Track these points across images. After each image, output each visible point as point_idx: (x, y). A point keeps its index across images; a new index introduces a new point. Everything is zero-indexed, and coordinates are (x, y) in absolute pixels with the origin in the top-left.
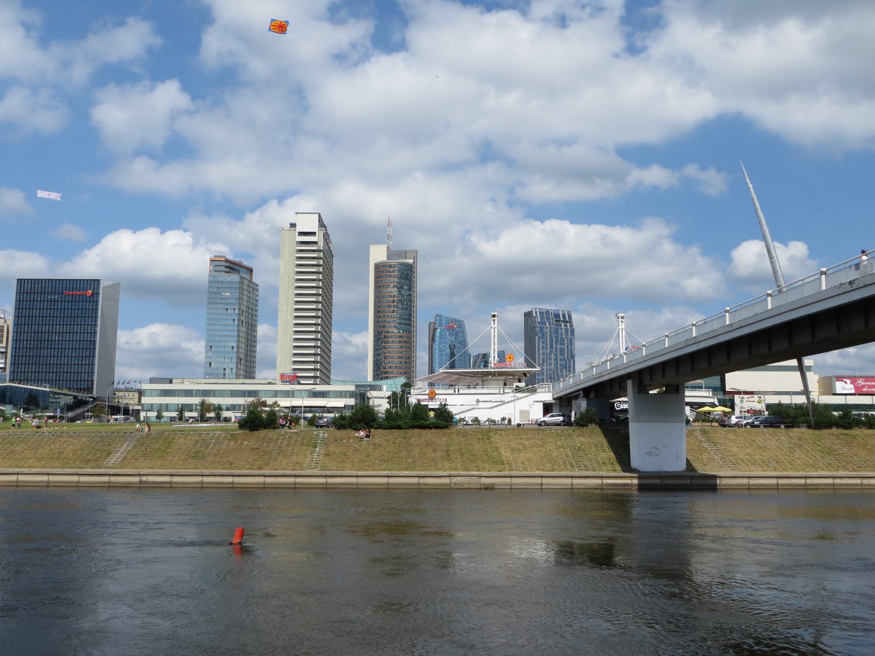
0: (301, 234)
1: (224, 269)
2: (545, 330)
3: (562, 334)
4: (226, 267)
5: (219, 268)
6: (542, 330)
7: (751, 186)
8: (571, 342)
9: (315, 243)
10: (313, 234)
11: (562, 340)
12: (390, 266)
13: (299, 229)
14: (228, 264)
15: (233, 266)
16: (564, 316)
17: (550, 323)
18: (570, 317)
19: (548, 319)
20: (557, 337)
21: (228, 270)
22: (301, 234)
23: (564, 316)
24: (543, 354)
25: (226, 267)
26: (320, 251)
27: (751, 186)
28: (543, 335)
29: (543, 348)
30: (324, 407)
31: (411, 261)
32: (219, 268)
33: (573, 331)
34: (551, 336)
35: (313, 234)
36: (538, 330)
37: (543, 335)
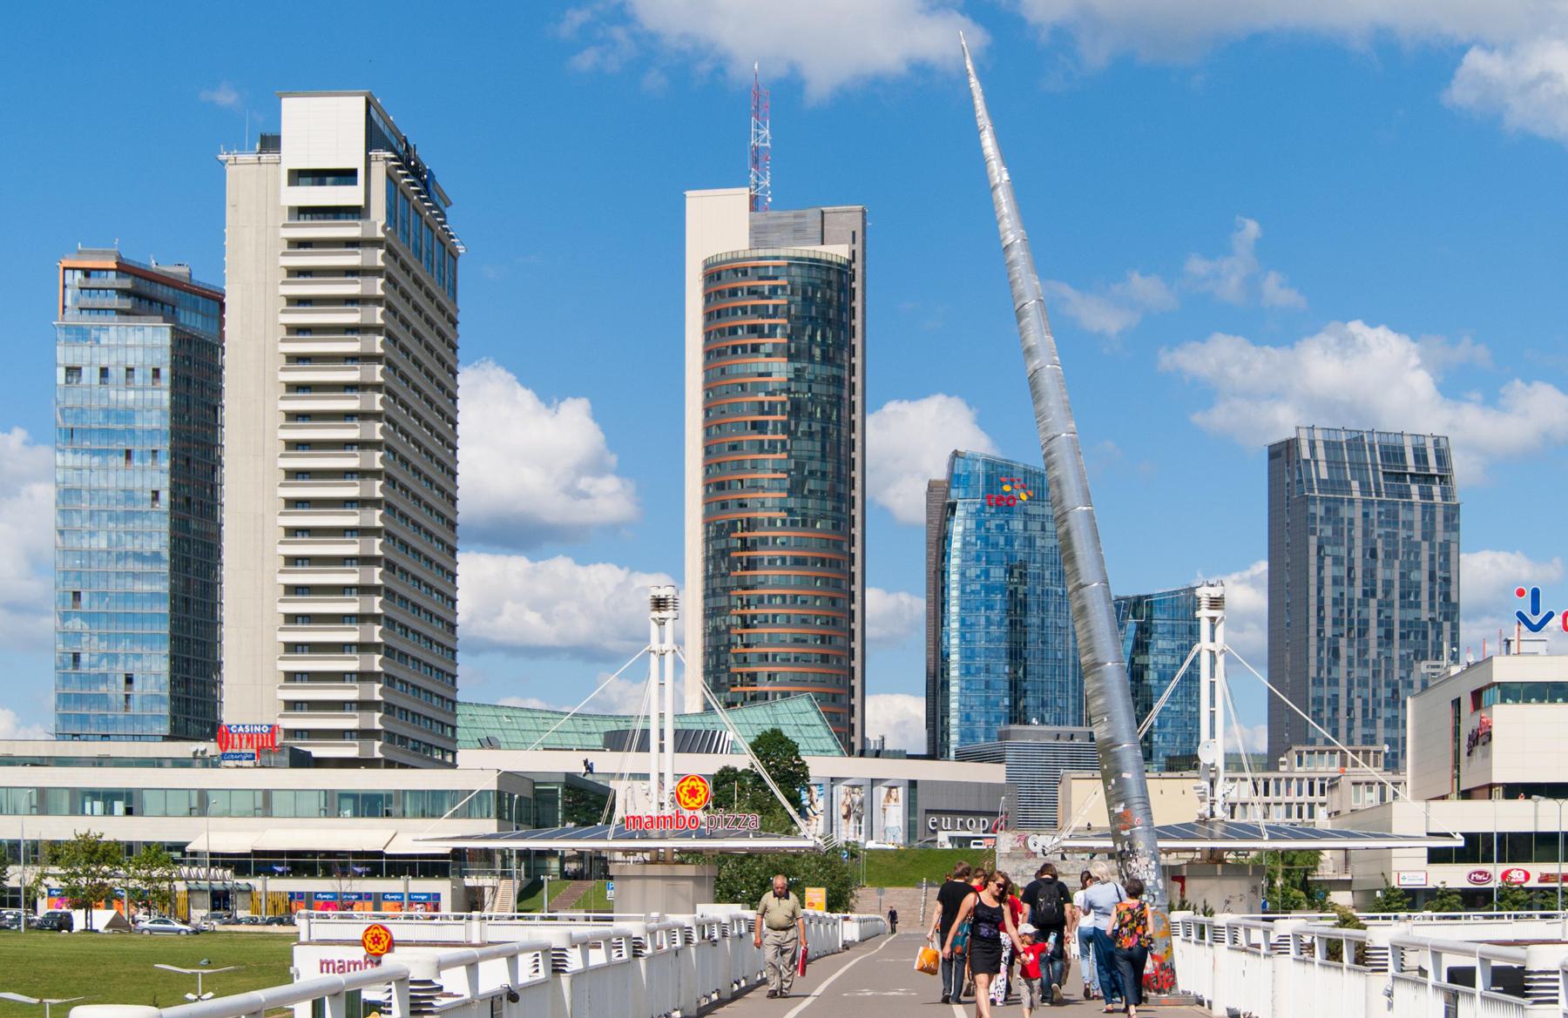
0: (299, 176)
1: (115, 301)
2: (1345, 512)
3: (1409, 525)
4: (123, 293)
5: (99, 301)
6: (1332, 513)
7: (999, 174)
8: (1446, 556)
10: (345, 176)
11: (1413, 548)
12: (760, 272)
13: (295, 155)
14: (127, 283)
15: (146, 287)
16: (1421, 456)
17: (1364, 488)
18: (1442, 458)
19: (1359, 467)
20: (1390, 538)
21: (127, 304)
22: (299, 176)
23: (1421, 456)
24: (1336, 602)
25: (123, 293)
26: (374, 243)
27: (999, 174)
28: (1337, 532)
29: (1336, 581)
30: (379, 854)
31: (839, 251)
32: (99, 301)
33: (1452, 514)
34: (1366, 533)
35: (345, 176)
36: (1319, 510)
37: (1337, 532)
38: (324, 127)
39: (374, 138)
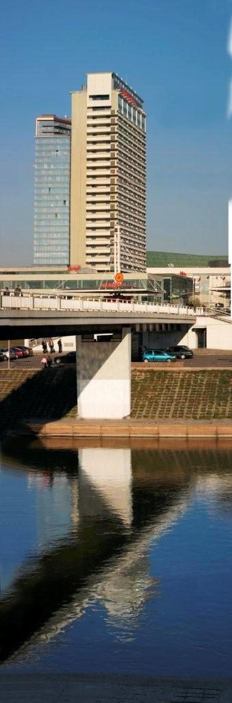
9: (109, 107)
10: (106, 97)
35: (106, 97)
38: (100, 82)
39: (115, 86)
